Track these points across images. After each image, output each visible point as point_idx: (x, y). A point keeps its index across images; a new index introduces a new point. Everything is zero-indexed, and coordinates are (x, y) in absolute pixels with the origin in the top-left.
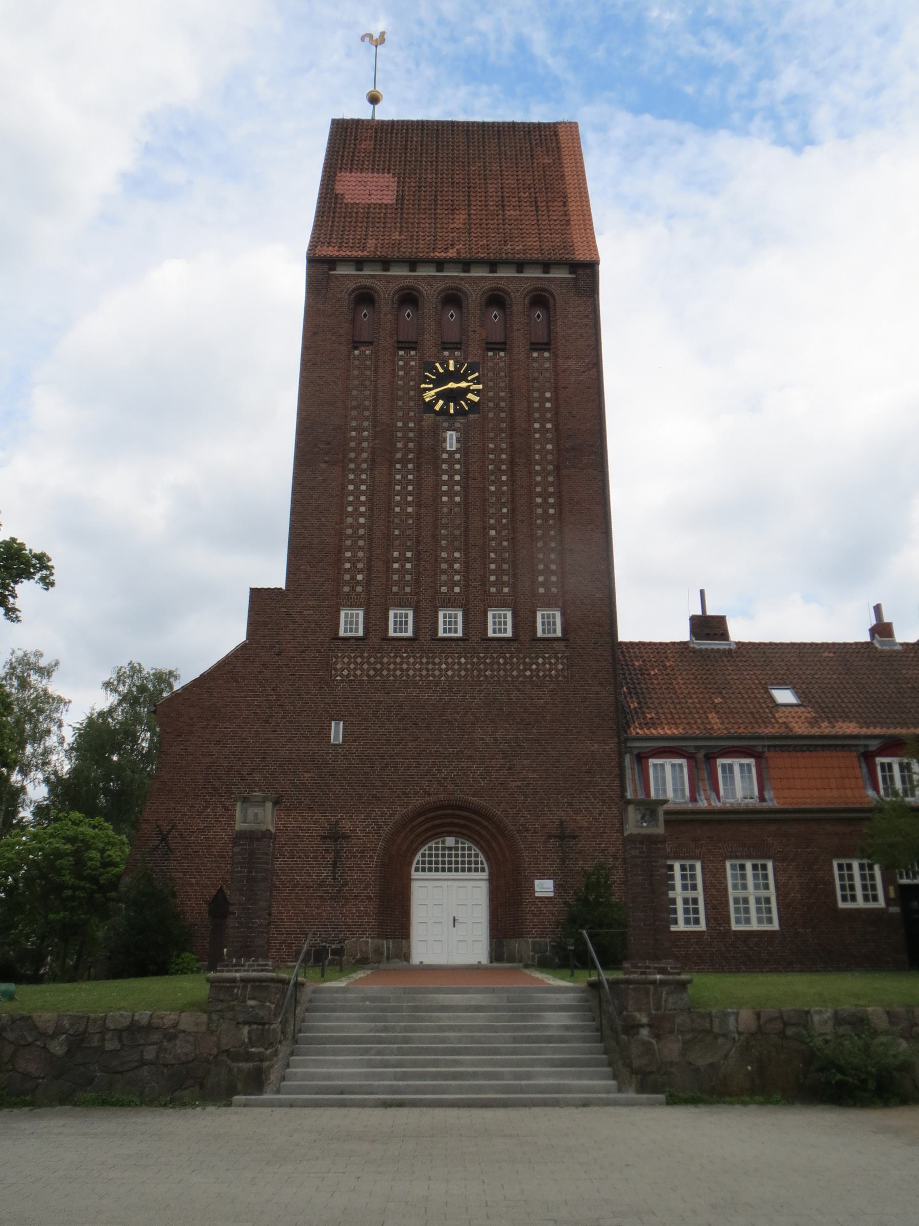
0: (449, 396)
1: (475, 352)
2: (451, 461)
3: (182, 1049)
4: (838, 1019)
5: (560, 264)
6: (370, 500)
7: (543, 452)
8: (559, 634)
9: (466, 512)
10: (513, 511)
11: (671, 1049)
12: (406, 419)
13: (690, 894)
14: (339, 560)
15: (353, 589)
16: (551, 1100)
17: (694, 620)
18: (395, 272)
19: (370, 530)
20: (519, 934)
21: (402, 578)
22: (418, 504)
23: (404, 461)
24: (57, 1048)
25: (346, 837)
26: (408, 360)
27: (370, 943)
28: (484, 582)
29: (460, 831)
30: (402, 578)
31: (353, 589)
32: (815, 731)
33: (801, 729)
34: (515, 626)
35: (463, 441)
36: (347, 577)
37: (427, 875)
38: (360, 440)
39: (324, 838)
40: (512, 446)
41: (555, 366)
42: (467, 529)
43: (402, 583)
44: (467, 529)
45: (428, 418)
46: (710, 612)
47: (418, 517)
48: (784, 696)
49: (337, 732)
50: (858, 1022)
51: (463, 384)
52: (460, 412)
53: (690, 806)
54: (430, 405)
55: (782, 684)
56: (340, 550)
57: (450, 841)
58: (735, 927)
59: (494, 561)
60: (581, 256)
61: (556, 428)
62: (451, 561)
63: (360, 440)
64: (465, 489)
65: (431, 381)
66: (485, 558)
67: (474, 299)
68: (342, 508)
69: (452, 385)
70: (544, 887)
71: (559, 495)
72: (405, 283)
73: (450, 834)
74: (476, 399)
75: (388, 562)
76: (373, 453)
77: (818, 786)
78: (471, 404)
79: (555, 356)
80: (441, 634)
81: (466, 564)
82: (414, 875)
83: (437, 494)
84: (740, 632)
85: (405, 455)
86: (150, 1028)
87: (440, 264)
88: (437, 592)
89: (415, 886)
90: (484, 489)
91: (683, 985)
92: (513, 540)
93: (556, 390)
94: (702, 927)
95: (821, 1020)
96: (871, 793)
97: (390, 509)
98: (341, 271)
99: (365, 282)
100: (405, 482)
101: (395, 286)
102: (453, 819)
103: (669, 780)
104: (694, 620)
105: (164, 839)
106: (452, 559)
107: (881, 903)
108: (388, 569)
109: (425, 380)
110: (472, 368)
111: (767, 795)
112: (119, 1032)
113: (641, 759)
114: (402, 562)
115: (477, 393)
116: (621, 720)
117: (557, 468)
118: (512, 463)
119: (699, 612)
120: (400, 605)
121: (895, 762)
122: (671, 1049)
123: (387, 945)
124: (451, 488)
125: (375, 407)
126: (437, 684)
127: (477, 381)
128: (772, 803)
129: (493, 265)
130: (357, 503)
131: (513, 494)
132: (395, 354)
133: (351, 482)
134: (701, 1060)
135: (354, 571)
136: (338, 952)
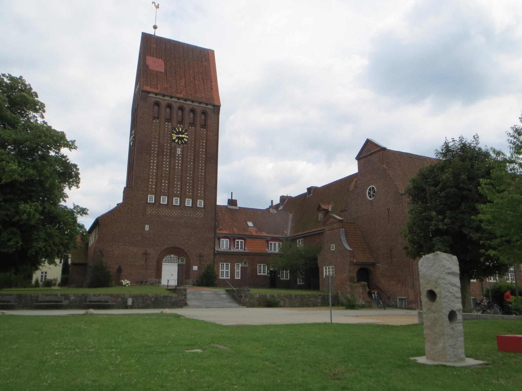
0: (179, 138)
1: (187, 126)
2: (179, 157)
3: (173, 300)
4: (270, 296)
5: (210, 104)
6: (157, 165)
7: (202, 157)
8: (203, 206)
9: (182, 172)
10: (194, 173)
11: (247, 300)
12: (167, 143)
13: (227, 270)
14: (149, 181)
15: (152, 190)
16: (231, 307)
17: (229, 200)
18: (166, 98)
19: (157, 174)
20: (189, 278)
21: (165, 188)
22: (170, 168)
23: (166, 155)
24: (153, 299)
25: (149, 254)
26: (168, 125)
27: (154, 280)
28: (185, 191)
29: (175, 254)
30: (165, 188)
31: (152, 190)
32: (257, 234)
33: (254, 234)
34: (192, 204)
35: (182, 151)
36: (150, 186)
37: (166, 264)
38: (155, 148)
39: (143, 254)
40: (194, 155)
41: (207, 133)
42: (182, 176)
43: (165, 189)
44: (182, 176)
45: (173, 144)
46: (233, 199)
47: (170, 171)
48: (250, 224)
49: (147, 228)
50: (273, 296)
51: (184, 136)
52: (182, 143)
53: (229, 251)
54: (174, 140)
55: (250, 220)
56: (149, 178)
57: (172, 256)
58: (236, 278)
59: (188, 186)
60: (216, 104)
61: (206, 151)
62: (177, 185)
63: (155, 148)
64: (182, 165)
65: (175, 133)
66: (186, 184)
67: (187, 110)
68: (150, 166)
69: (180, 136)
70: (195, 268)
71: (205, 170)
72: (169, 102)
73: (172, 254)
74: (186, 140)
75: (161, 183)
76: (158, 152)
77: (255, 247)
78: (185, 142)
79: (207, 131)
80: (174, 204)
81: (181, 186)
82: (163, 263)
83: (175, 166)
84: (240, 204)
85: (167, 153)
86: (168, 296)
87: (179, 99)
88: (173, 193)
89: (163, 266)
90: (187, 166)
91: (249, 290)
92: (193, 181)
93: (207, 140)
94: (229, 278)
95: (268, 296)
96: (267, 249)
97: (162, 168)
98: (151, 95)
99: (159, 100)
100: (166, 161)
101: (166, 102)
102: (176, 251)
103: (224, 245)
104: (229, 200)
105: (101, 253)
106: (178, 184)
107: (266, 274)
108: (161, 185)
109: (173, 133)
110: (186, 131)
111: (246, 249)
112: (163, 297)
113: (219, 239)
114: (165, 184)
115: (187, 139)
116: (215, 228)
117: (206, 162)
118: (194, 160)
119: (230, 198)
120: (164, 195)
121: (273, 243)
122: (247, 300)
123: (157, 280)
124: (178, 165)
125: (159, 139)
126: (173, 217)
127: (187, 135)
128: (247, 251)
129: (193, 102)
130: (153, 166)
131: (194, 168)
132: (165, 123)
133: (152, 160)
134: (251, 301)
135: (152, 185)
136: (146, 282)
